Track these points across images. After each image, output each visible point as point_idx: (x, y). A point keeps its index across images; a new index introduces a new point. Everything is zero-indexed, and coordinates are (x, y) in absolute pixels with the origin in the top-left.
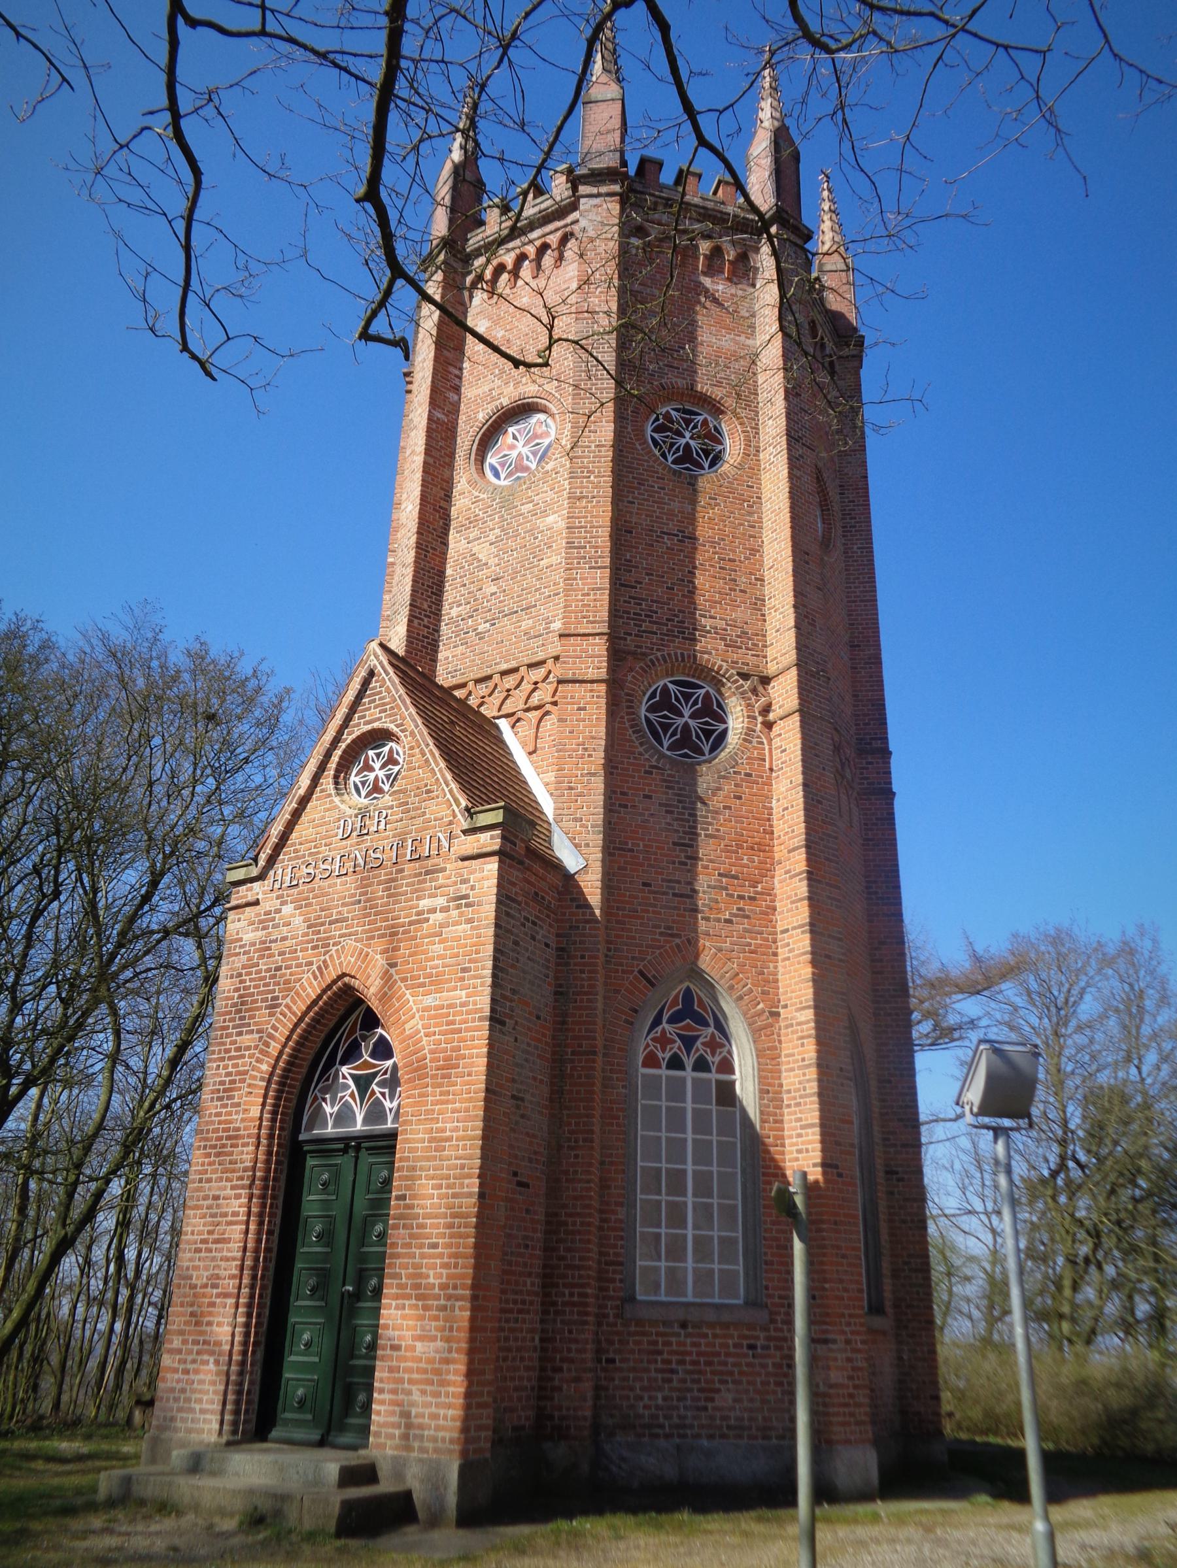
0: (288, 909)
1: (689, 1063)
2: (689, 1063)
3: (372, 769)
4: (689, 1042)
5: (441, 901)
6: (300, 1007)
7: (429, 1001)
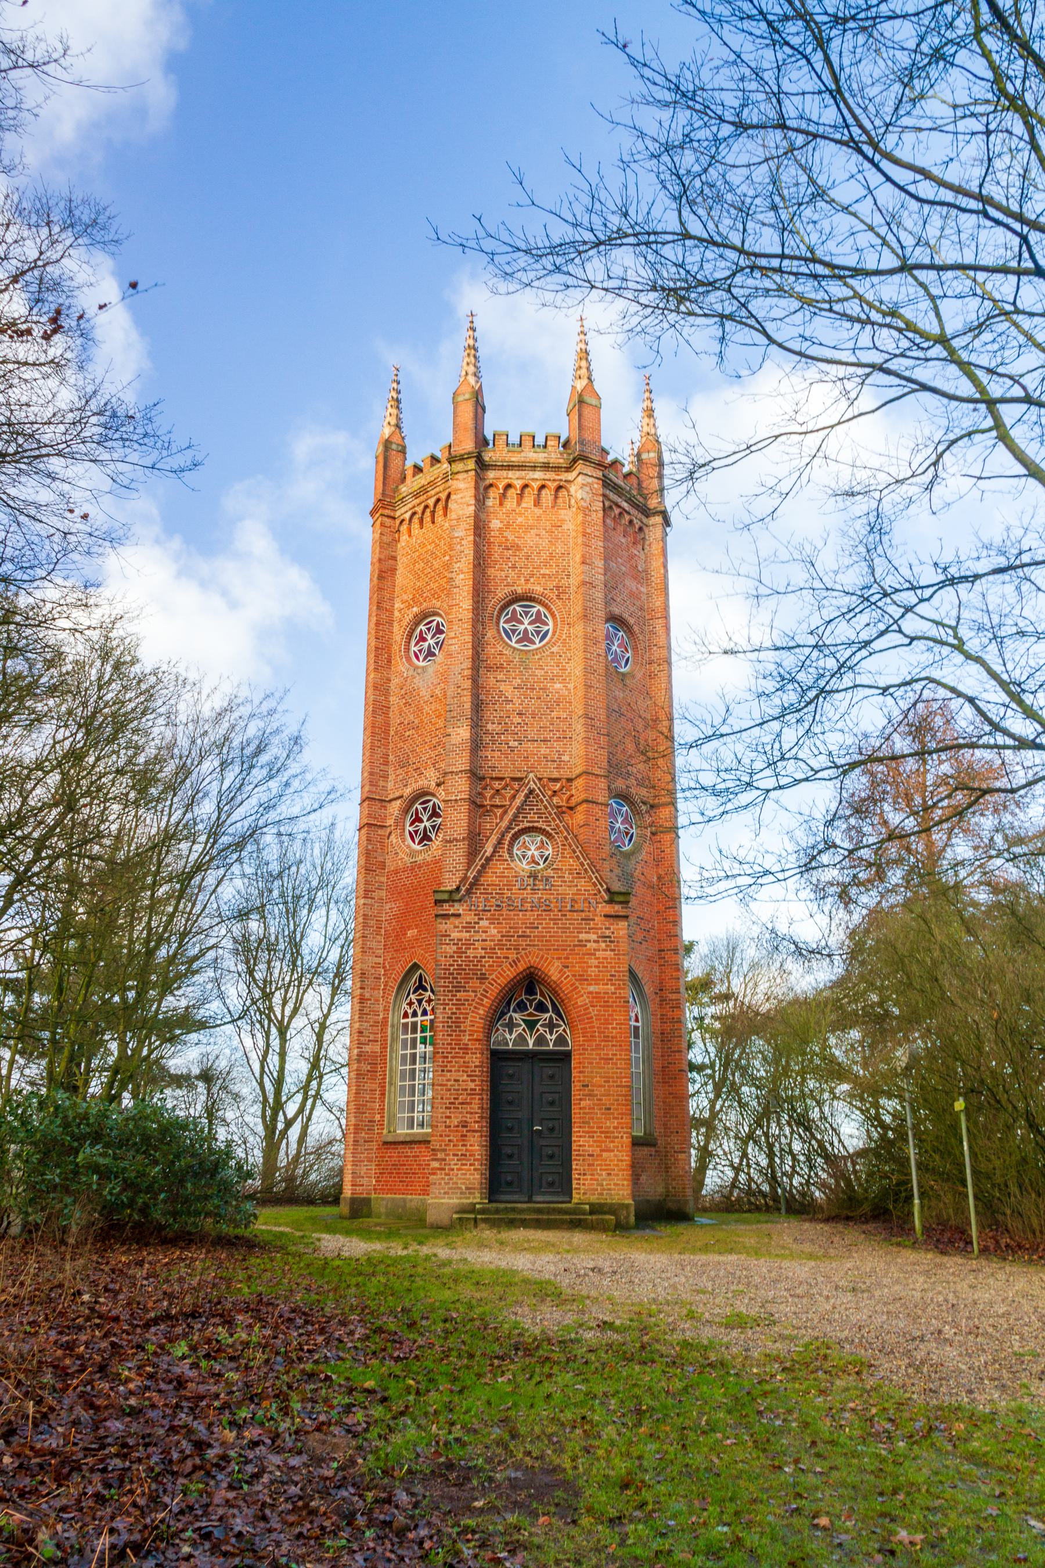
0: (484, 923)
1: (419, 1013)
2: (419, 1013)
3: (421, 821)
4: (420, 1001)
5: (594, 937)
6: (502, 981)
7: (592, 988)
